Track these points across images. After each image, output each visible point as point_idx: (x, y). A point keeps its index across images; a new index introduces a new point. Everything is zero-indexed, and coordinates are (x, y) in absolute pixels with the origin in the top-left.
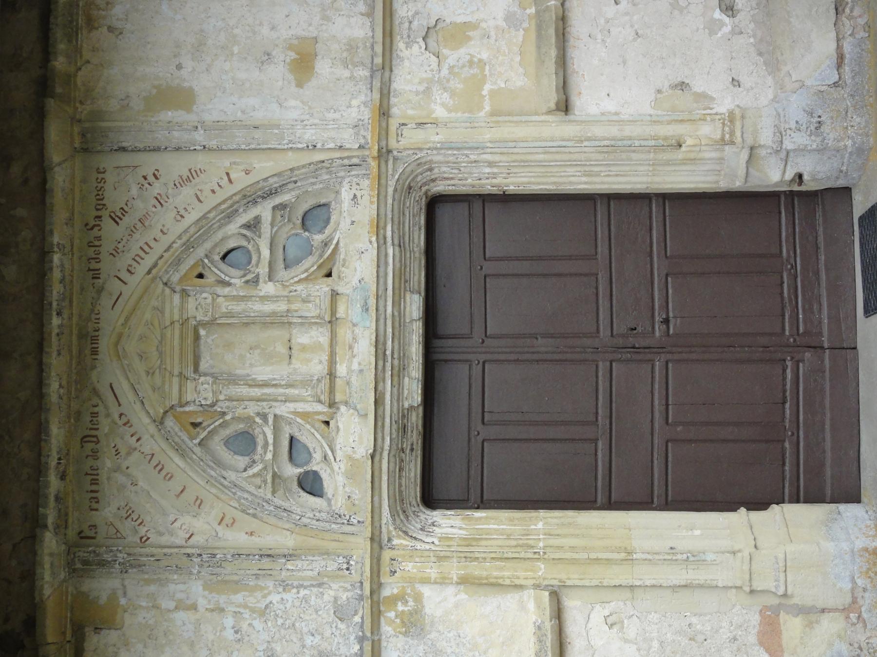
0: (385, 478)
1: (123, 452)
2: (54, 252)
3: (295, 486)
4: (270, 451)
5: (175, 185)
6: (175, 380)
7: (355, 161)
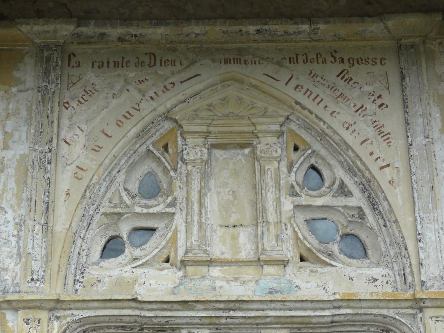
0: (116, 312)
1: (143, 86)
2: (311, 25)
3: (111, 233)
4: (142, 210)
5: (375, 122)
6: (204, 129)
7: (409, 279)
